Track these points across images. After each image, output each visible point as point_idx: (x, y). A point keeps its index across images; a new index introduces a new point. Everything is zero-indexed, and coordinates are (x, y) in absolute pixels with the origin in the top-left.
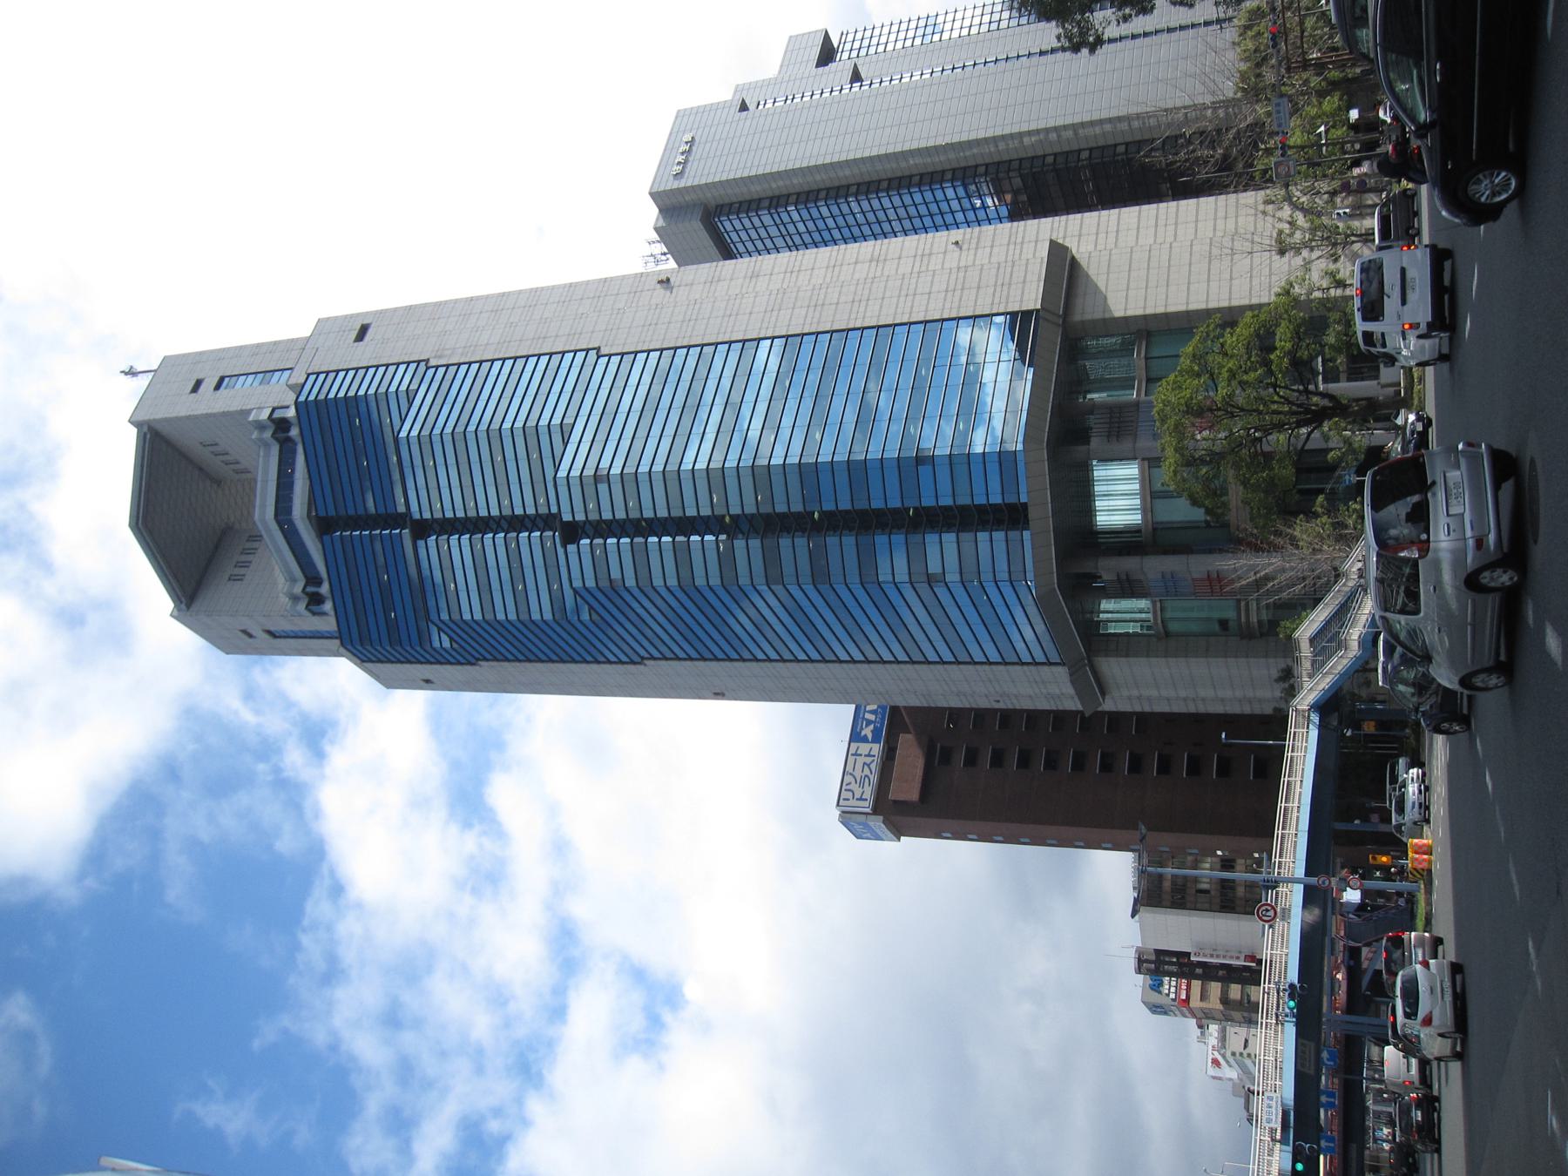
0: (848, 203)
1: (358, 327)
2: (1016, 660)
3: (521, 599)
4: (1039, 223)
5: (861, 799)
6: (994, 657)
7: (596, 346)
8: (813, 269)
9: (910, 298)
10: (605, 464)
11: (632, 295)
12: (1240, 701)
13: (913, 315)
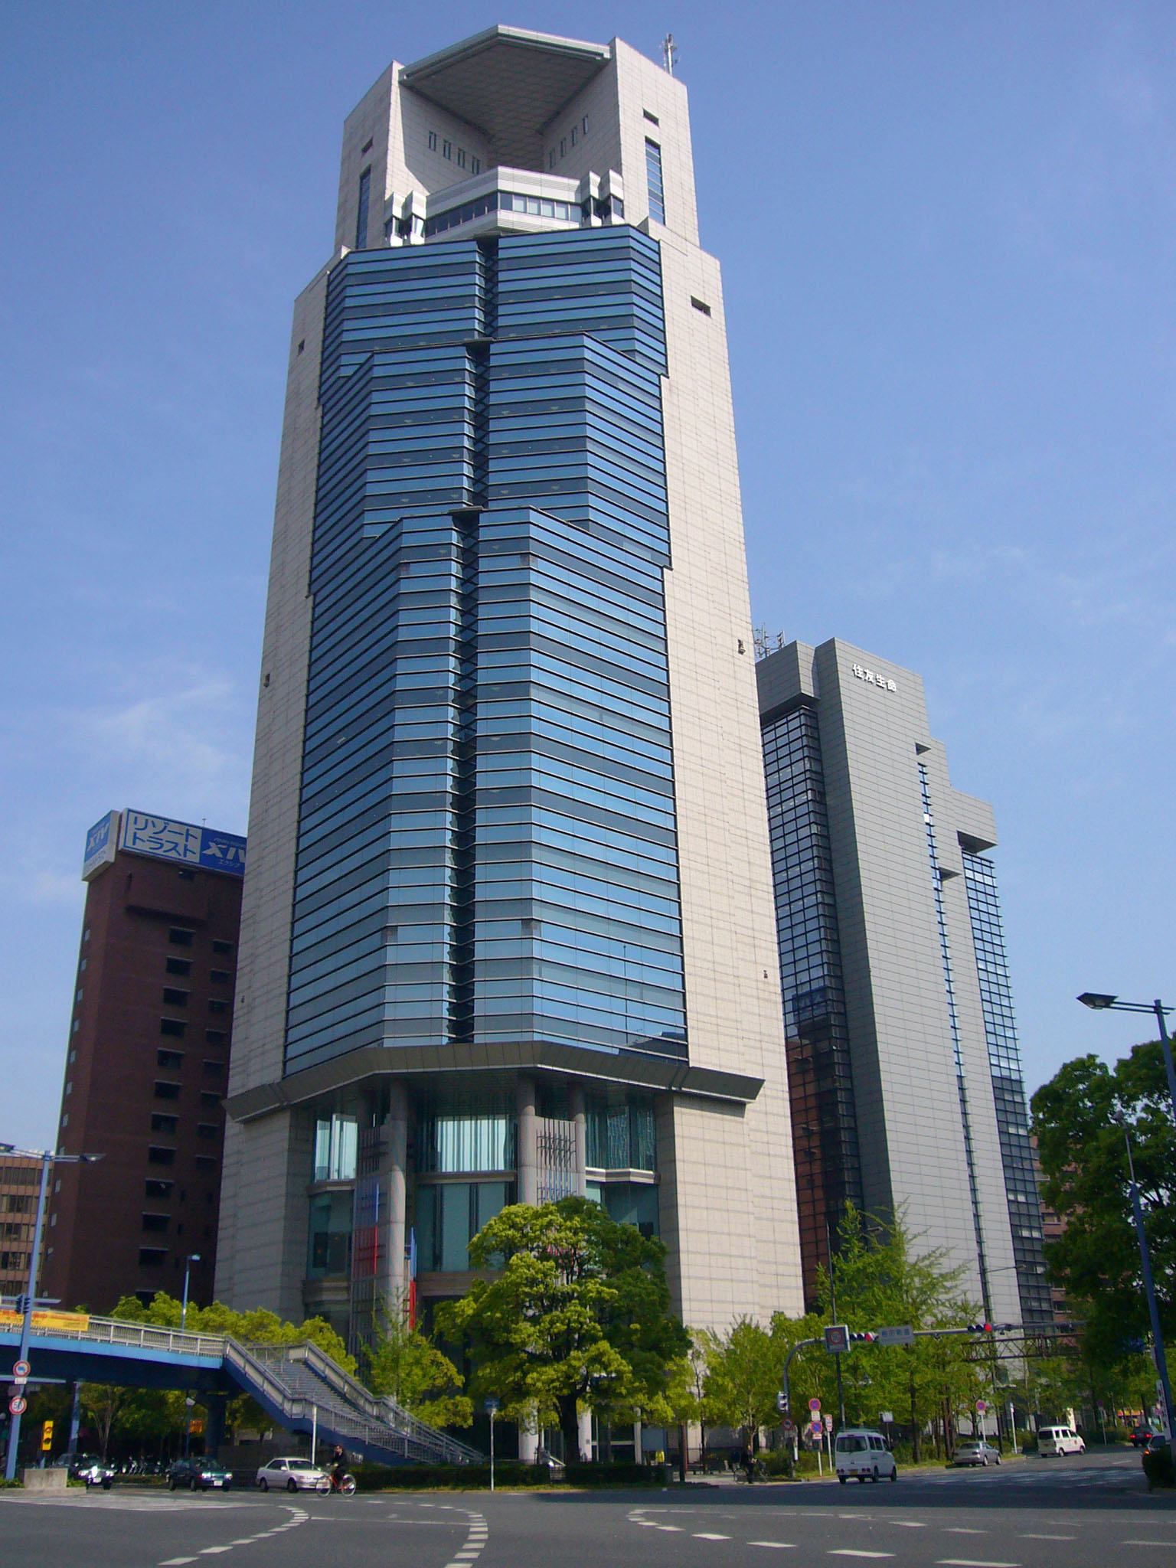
0: (816, 893)
2: (293, 987)
3: (395, 420)
5: (135, 837)
8: (752, 912)
9: (708, 921)
11: (724, 570)
12: (235, 1216)
13: (695, 1031)
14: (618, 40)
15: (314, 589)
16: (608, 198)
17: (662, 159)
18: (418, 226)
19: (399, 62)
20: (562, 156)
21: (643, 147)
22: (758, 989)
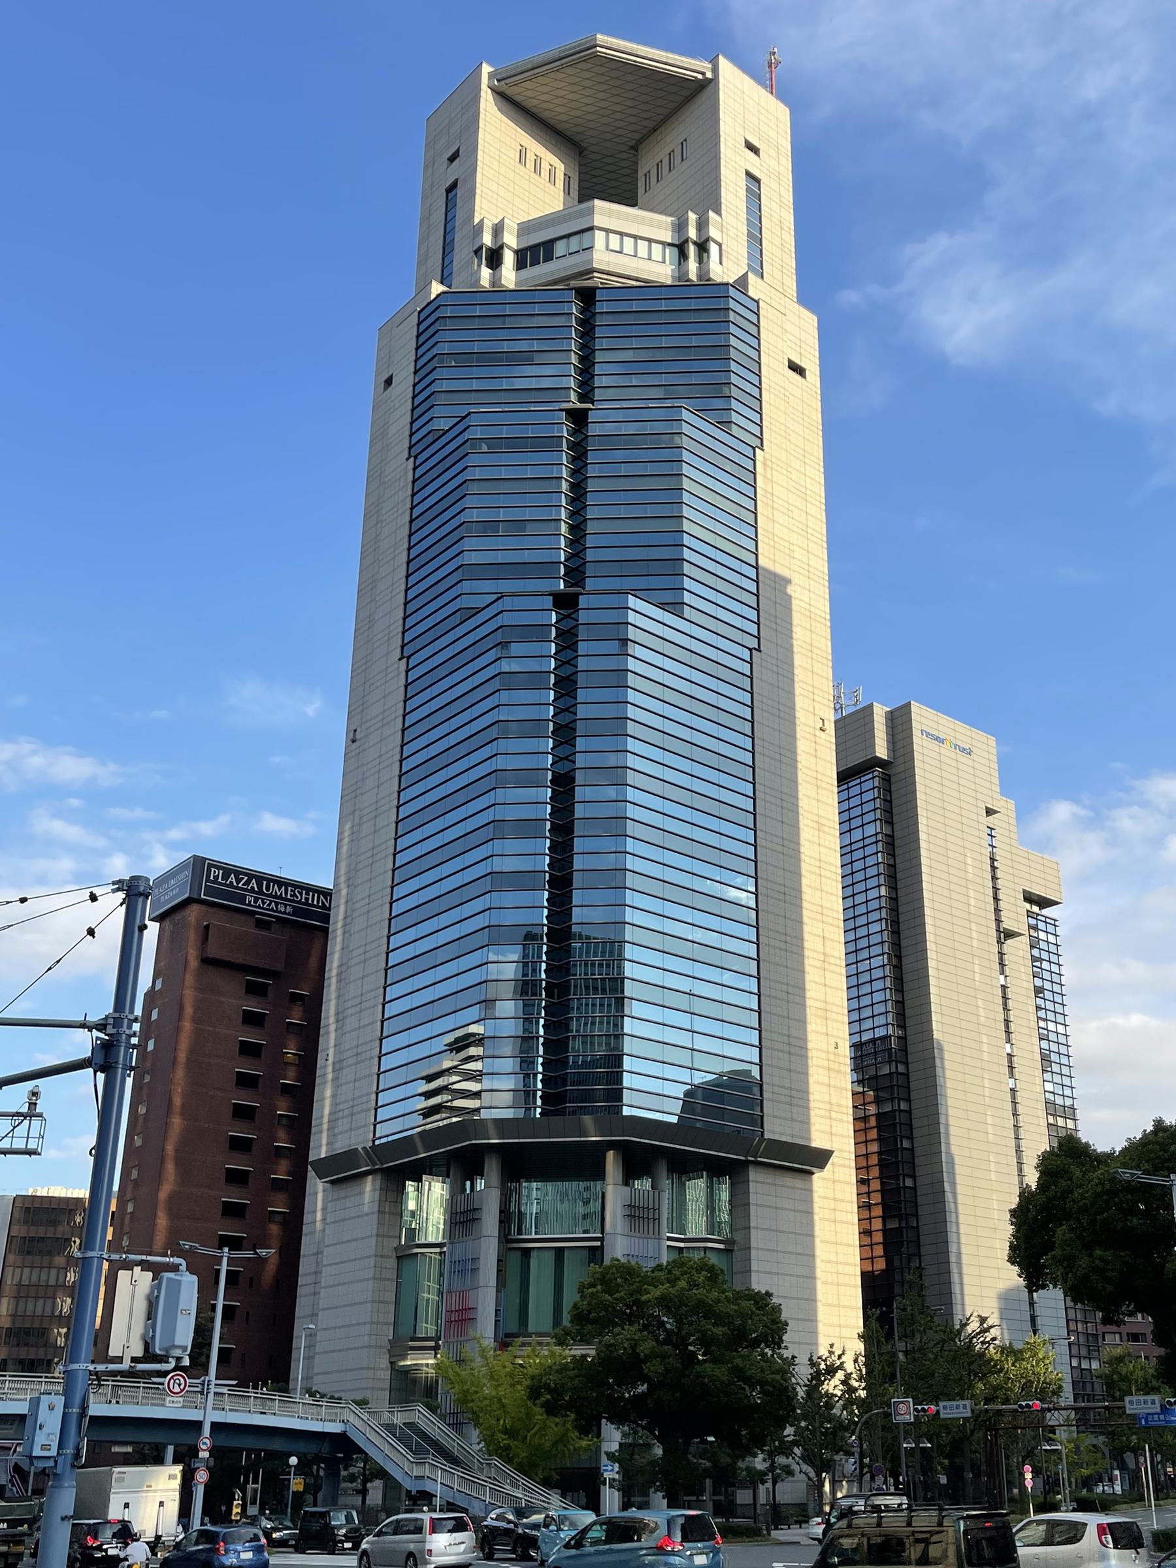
1: (803, 365)
4: (850, 1183)
6: (394, 959)
7: (762, 648)
8: (825, 985)
10: (639, 651)
14: (721, 58)
15: (414, 451)
16: (707, 240)
17: (763, 240)
18: (509, 258)
19: (490, 63)
21: (742, 182)
22: (828, 1060)
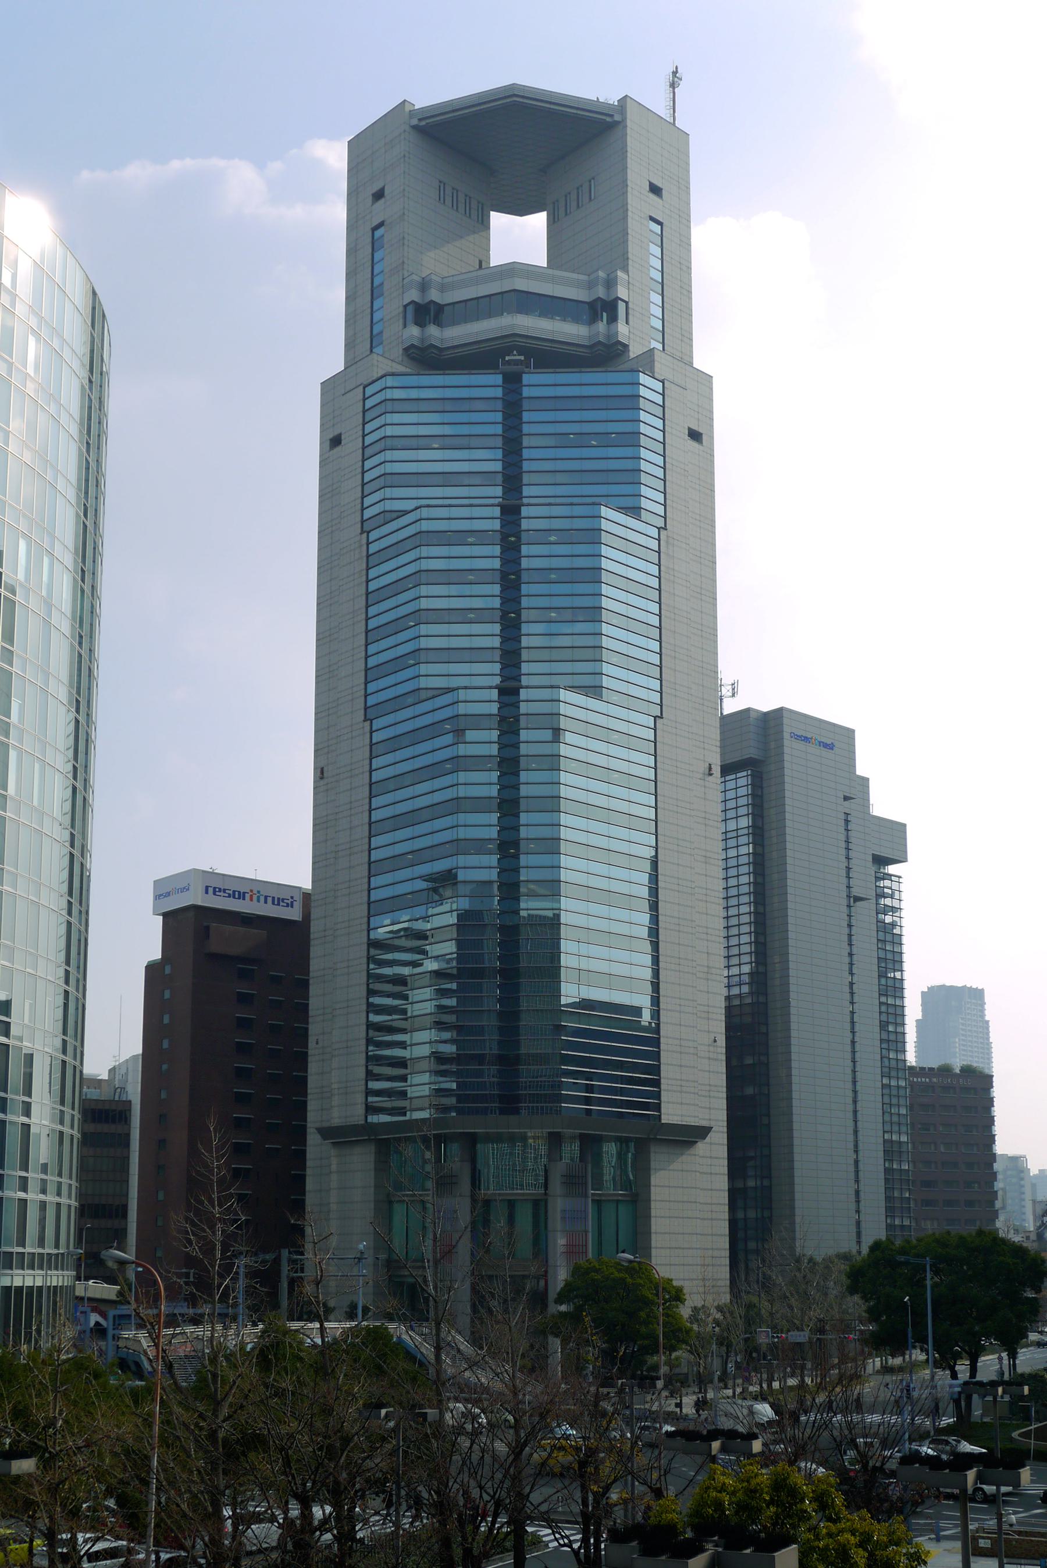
7: (668, 527)
20: (566, 214)
